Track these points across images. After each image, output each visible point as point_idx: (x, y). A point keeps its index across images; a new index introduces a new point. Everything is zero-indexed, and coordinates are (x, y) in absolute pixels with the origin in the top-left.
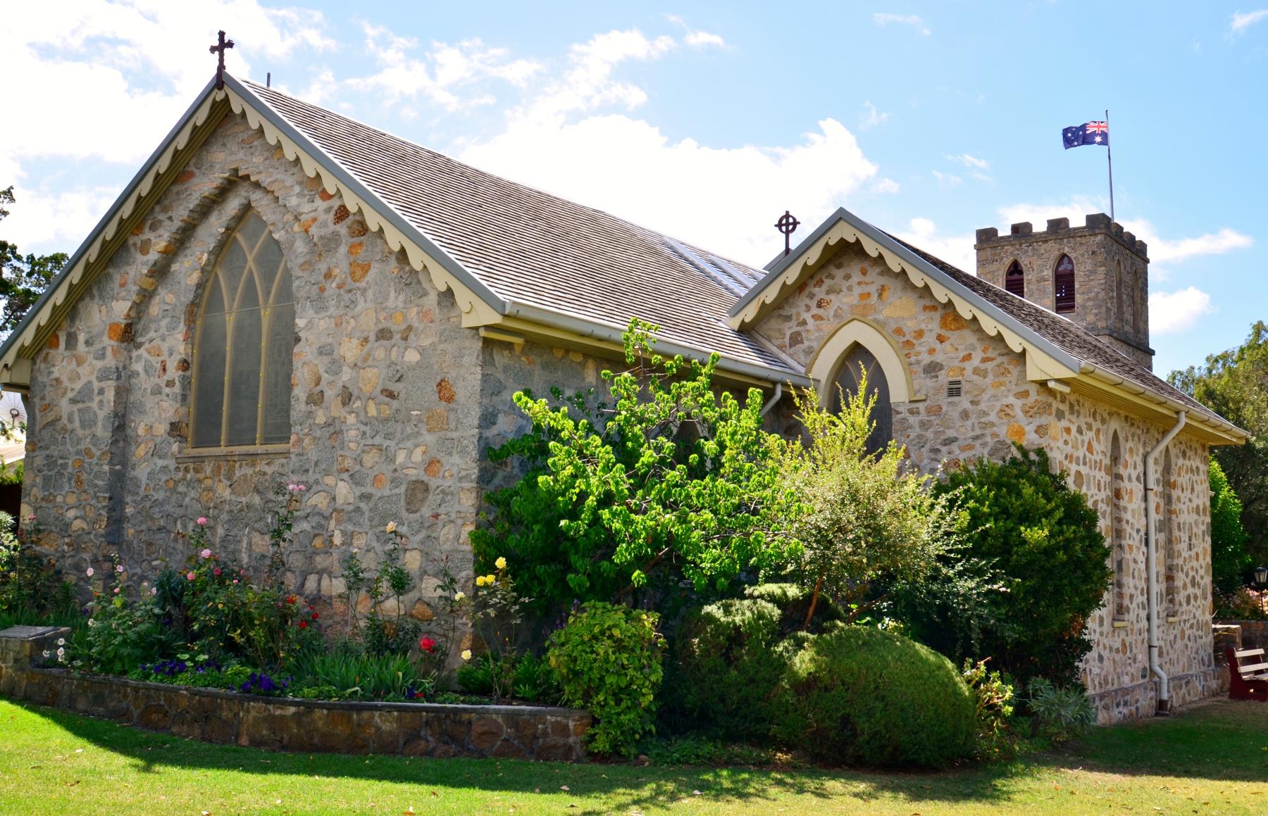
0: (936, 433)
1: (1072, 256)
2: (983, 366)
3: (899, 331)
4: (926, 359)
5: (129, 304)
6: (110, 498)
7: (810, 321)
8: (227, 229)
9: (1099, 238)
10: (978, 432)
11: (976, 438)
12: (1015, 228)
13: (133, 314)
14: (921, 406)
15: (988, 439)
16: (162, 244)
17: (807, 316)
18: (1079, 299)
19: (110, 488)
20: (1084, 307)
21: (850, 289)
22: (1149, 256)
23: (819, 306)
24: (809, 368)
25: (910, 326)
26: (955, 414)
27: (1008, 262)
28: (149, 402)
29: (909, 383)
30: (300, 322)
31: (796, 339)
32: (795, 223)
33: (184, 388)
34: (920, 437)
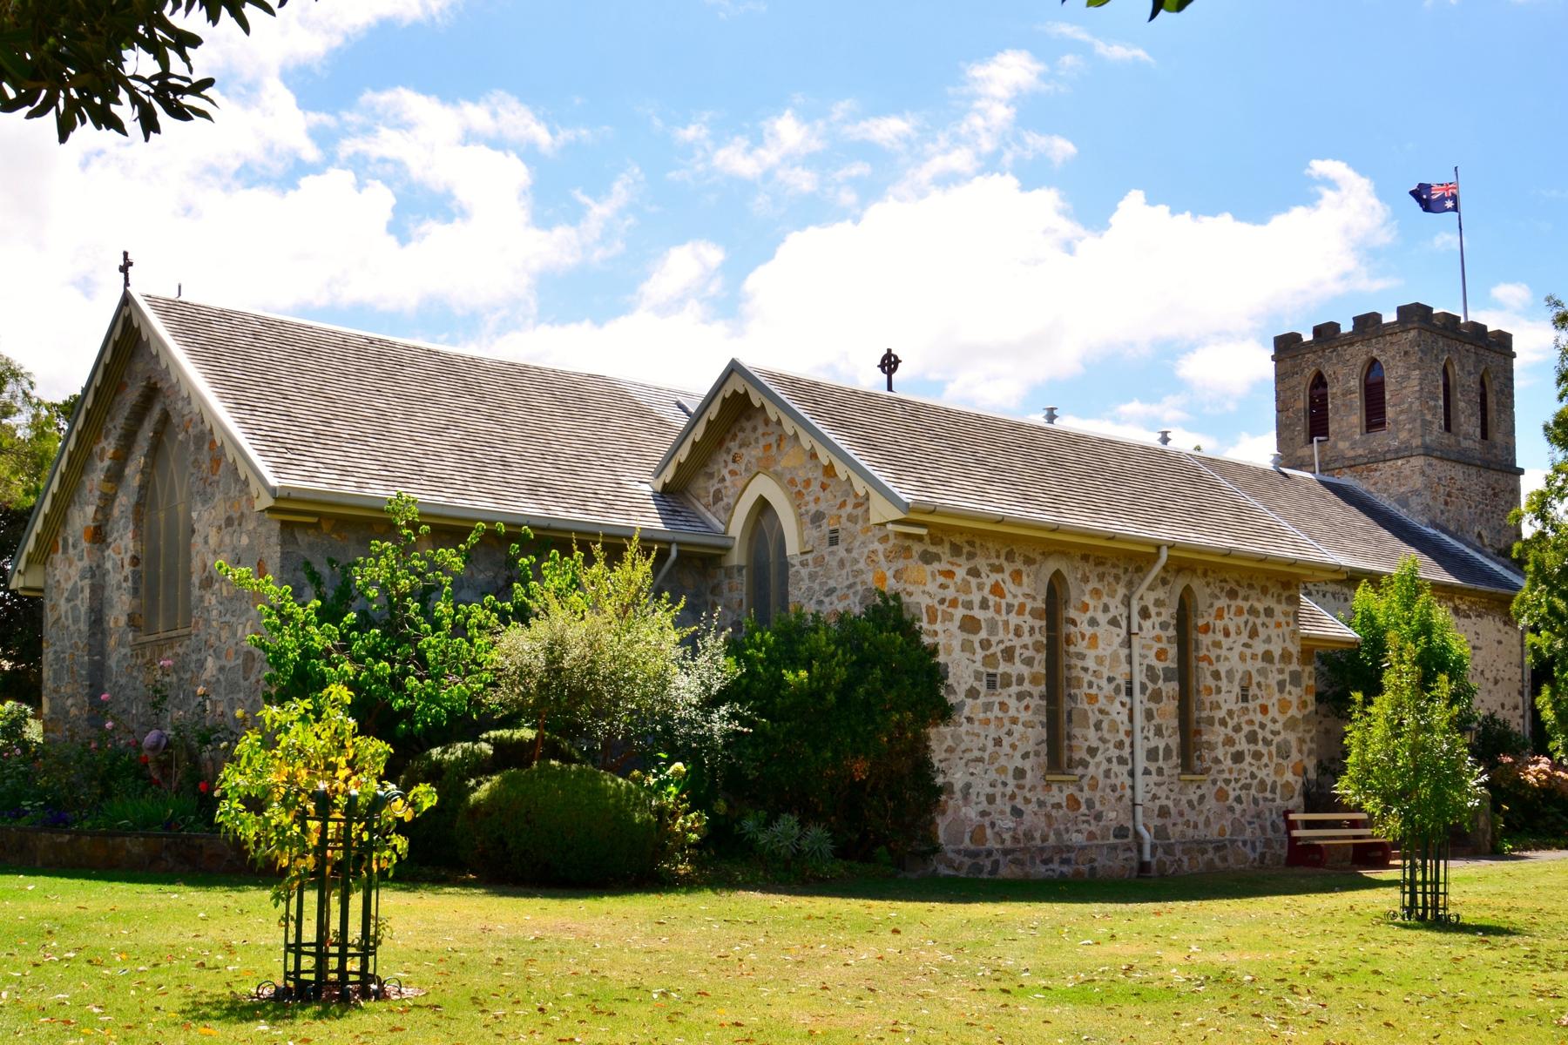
0: (821, 584)
1: (1382, 359)
2: (855, 512)
3: (792, 482)
4: (812, 508)
5: (93, 508)
6: (91, 686)
7: (728, 477)
8: (155, 433)
9: (1413, 333)
10: (851, 580)
11: (850, 587)
12: (1318, 331)
13: (100, 517)
14: (809, 557)
15: (859, 587)
16: (110, 451)
17: (725, 472)
18: (1390, 412)
19: (91, 675)
20: (1396, 422)
21: (757, 441)
22: (1514, 349)
23: (734, 461)
24: (727, 524)
25: (801, 475)
26: (834, 564)
27: (1309, 373)
28: (115, 596)
29: (801, 534)
30: (194, 515)
31: (718, 497)
32: (897, 361)
33: (135, 582)
34: (809, 589)
